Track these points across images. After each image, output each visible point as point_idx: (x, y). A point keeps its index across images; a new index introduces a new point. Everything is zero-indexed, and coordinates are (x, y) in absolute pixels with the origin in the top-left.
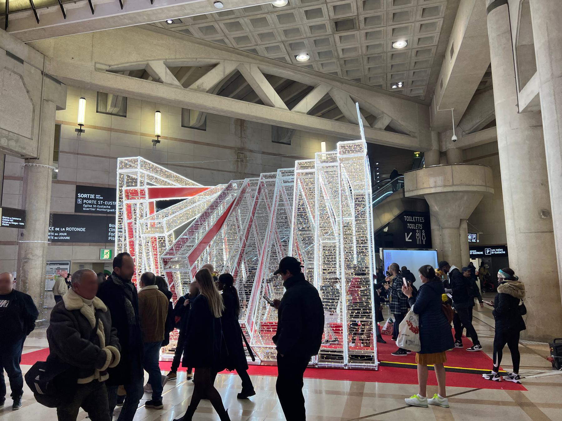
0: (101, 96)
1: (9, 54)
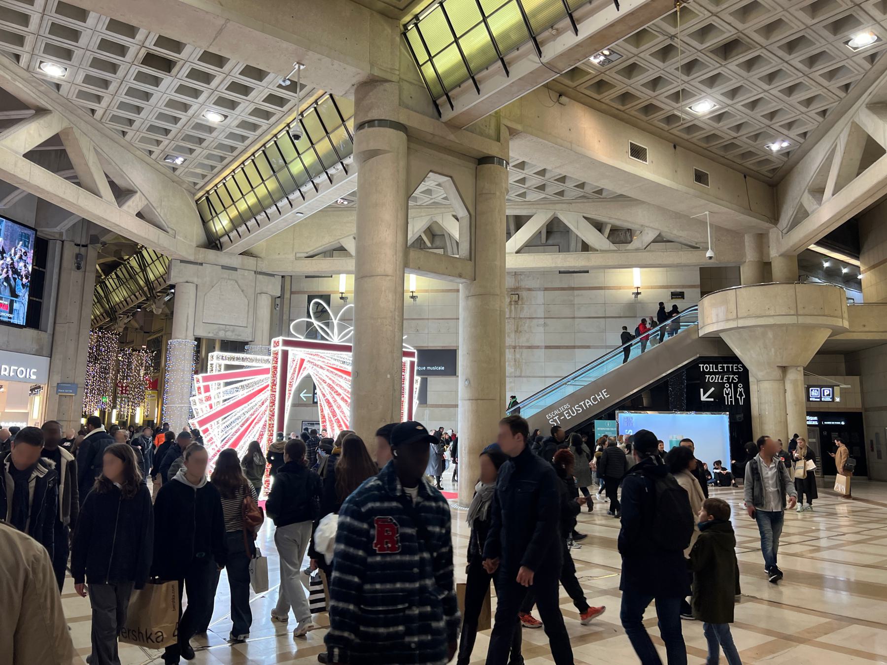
1: (224, 267)
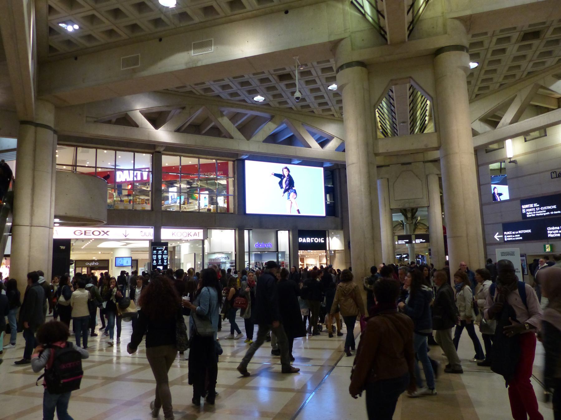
0: (525, 134)
1: (403, 164)
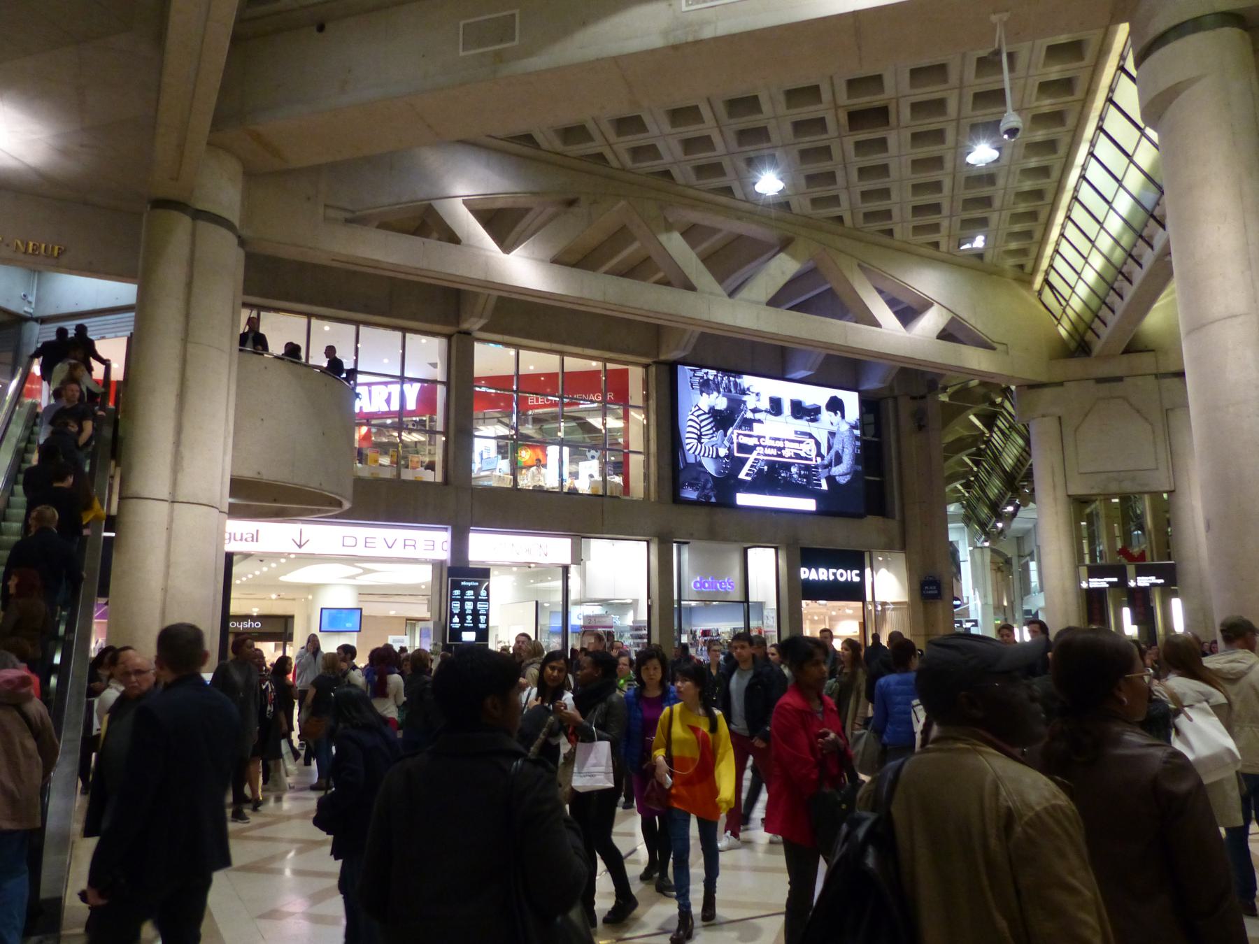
1: (1100, 381)
